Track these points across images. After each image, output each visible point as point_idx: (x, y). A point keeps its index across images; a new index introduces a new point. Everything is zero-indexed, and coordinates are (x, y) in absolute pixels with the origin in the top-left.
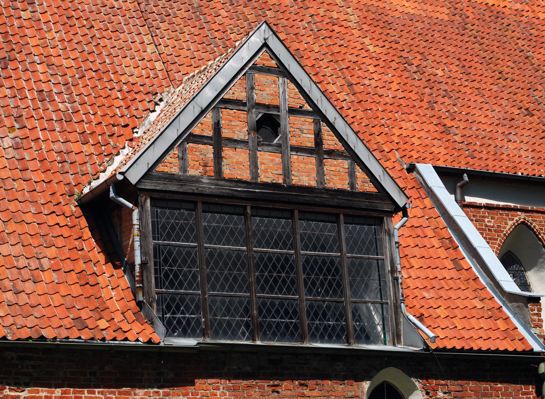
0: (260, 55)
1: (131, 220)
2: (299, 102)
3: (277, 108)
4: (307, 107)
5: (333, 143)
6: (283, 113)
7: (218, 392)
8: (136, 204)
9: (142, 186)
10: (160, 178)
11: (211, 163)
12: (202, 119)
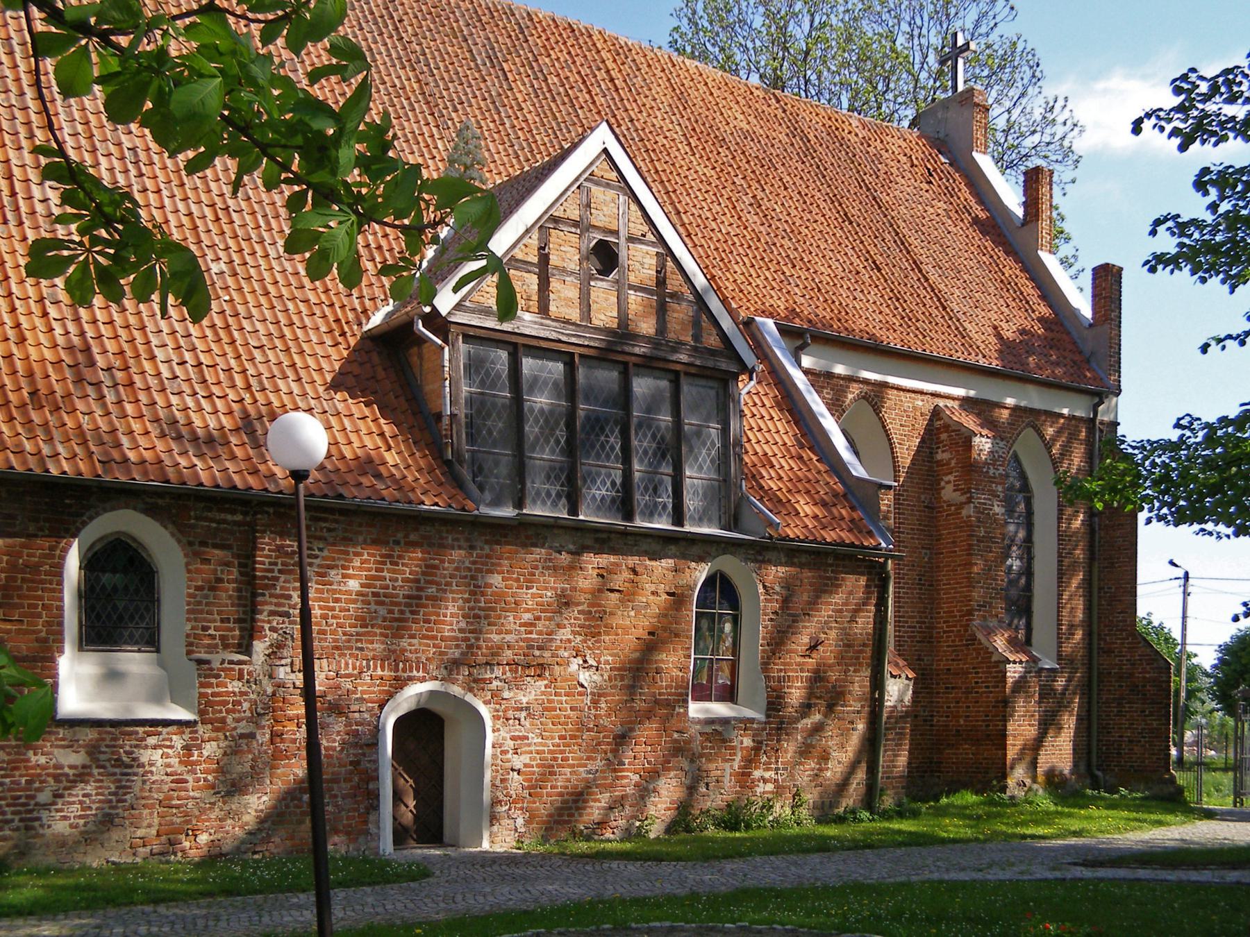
0: (598, 163)
1: (443, 361)
2: (640, 228)
3: (615, 233)
4: (650, 237)
5: (677, 283)
6: (622, 241)
7: (537, 572)
8: (446, 341)
9: (453, 319)
10: (473, 311)
11: (535, 298)
12: (526, 240)
